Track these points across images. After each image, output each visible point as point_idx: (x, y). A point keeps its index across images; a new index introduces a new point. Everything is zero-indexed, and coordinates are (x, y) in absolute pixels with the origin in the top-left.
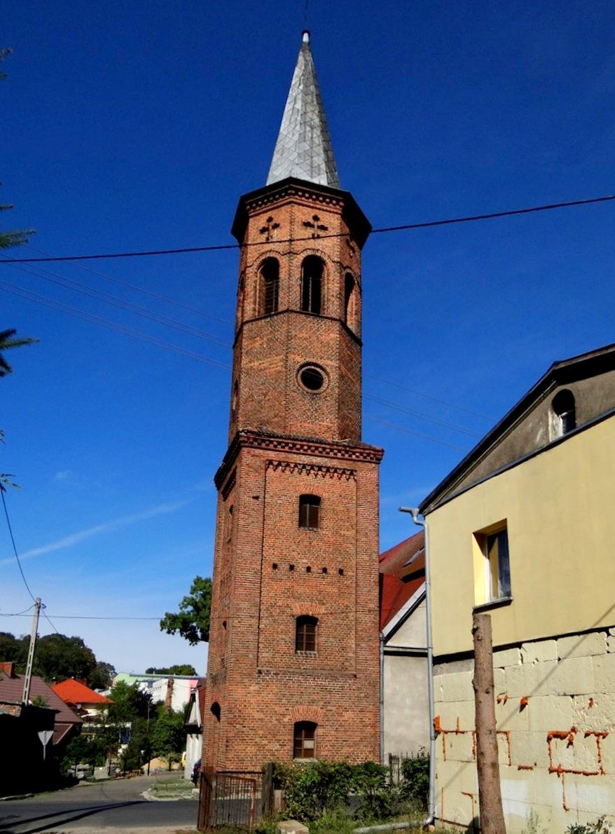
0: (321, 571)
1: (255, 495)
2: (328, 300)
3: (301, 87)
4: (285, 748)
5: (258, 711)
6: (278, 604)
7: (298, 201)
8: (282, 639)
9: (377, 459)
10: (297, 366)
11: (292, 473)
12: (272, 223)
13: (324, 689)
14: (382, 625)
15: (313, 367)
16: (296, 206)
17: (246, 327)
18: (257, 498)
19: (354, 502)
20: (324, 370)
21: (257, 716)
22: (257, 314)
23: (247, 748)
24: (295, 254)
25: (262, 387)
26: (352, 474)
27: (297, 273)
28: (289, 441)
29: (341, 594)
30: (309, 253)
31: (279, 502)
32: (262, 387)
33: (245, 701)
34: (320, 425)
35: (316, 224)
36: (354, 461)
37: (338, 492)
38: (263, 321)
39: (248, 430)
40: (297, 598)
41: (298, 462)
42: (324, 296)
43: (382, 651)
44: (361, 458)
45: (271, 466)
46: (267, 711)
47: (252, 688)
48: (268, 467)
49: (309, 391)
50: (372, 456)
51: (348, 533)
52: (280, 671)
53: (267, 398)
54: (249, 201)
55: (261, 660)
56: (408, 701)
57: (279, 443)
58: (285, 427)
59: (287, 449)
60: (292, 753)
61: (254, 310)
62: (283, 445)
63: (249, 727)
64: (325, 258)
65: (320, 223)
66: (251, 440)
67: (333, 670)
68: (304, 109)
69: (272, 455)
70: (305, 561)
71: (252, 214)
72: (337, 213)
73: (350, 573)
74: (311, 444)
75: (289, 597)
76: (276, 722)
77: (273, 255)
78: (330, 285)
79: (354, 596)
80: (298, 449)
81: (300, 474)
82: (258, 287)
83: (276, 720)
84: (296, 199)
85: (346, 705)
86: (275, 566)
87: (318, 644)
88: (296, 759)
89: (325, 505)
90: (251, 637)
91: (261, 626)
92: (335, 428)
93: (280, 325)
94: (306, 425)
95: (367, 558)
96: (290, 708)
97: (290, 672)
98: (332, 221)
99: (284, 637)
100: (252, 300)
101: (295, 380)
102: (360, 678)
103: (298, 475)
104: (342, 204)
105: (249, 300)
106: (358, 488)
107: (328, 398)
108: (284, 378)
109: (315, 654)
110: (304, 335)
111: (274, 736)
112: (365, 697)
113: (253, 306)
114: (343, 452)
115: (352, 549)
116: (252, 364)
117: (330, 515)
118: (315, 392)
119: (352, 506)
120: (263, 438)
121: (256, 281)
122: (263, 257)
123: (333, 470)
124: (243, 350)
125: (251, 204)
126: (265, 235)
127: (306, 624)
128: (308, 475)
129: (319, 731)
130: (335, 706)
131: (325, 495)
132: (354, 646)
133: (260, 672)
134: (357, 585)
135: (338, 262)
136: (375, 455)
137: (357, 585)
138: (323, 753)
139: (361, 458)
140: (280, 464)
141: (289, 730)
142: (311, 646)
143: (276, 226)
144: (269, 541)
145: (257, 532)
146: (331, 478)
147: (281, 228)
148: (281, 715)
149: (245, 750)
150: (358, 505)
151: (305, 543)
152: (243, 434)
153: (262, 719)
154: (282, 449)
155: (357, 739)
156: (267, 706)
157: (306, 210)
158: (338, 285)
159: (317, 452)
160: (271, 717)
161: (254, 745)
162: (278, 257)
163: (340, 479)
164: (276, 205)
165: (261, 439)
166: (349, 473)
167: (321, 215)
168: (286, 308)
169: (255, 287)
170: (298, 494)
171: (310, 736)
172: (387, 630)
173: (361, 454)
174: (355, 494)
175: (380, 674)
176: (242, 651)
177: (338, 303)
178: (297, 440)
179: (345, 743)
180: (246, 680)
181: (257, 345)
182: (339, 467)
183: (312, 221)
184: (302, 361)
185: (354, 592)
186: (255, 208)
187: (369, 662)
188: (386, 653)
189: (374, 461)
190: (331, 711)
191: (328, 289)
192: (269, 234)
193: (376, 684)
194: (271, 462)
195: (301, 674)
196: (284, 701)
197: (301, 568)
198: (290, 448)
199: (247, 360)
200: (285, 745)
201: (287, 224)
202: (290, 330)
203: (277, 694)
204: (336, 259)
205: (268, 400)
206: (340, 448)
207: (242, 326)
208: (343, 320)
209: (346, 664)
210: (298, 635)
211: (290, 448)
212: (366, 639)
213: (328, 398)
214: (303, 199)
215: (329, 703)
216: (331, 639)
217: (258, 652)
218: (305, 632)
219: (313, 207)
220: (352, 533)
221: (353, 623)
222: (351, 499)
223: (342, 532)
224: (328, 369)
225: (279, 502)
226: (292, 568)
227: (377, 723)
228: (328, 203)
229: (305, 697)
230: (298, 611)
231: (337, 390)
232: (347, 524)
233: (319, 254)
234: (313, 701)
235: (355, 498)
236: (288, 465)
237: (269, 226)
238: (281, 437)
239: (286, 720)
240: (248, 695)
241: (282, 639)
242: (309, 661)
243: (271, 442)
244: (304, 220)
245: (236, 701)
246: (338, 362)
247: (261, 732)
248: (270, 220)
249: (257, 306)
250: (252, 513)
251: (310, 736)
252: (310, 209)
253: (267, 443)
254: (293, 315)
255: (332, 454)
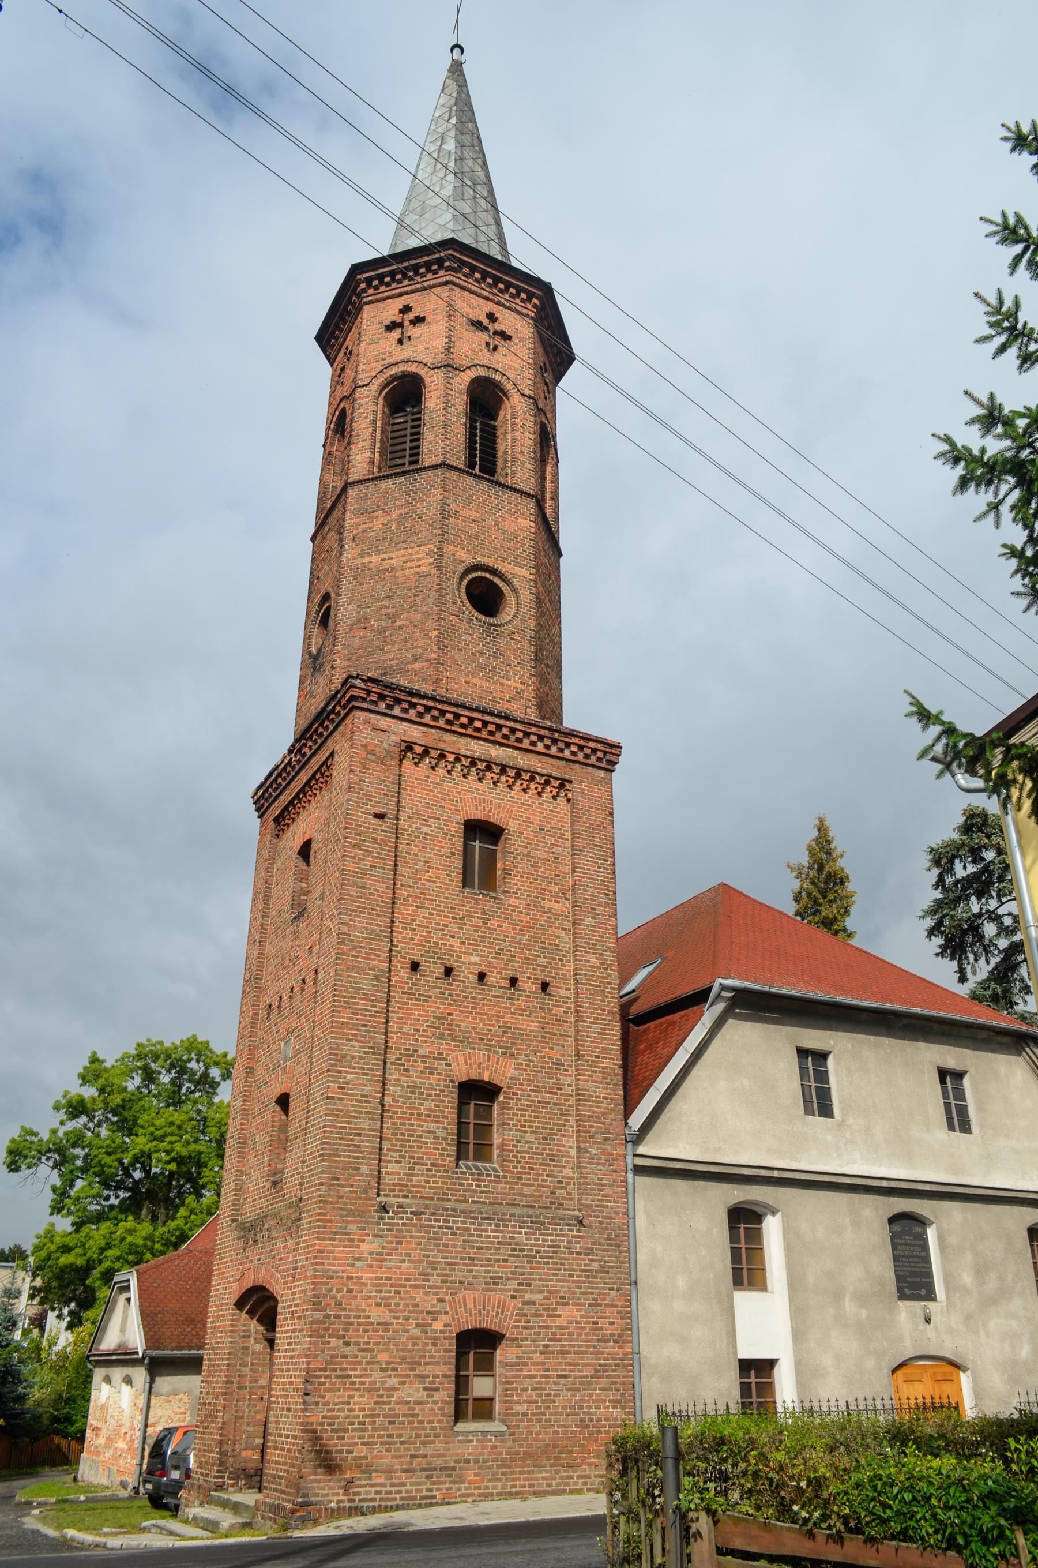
0: (506, 983)
1: (378, 810)
2: (514, 459)
3: (453, 121)
4: (437, 1396)
5: (378, 1305)
6: (421, 1051)
7: (462, 283)
8: (429, 1132)
9: (610, 762)
10: (461, 569)
11: (449, 772)
12: (411, 316)
13: (518, 1251)
14: (629, 1106)
15: (488, 575)
16: (458, 290)
17: (352, 493)
18: (380, 816)
19: (568, 844)
20: (507, 581)
21: (377, 1314)
22: (376, 470)
23: (351, 1397)
24: (456, 369)
25: (386, 602)
26: (562, 786)
27: (460, 403)
28: (448, 708)
29: (545, 1035)
30: (482, 372)
31: (425, 829)
32: (386, 602)
33: (350, 1278)
34: (502, 684)
35: (490, 327)
36: (567, 760)
37: (536, 819)
38: (390, 482)
39: (369, 678)
40: (463, 1040)
41: (463, 752)
42: (506, 452)
43: (630, 1166)
44: (580, 756)
45: (410, 755)
46: (397, 1305)
47: (365, 1247)
48: (404, 757)
49: (482, 617)
50: (600, 754)
51: (556, 906)
52: (427, 1206)
53: (398, 623)
54: (365, 275)
55: (386, 1180)
56: (681, 1282)
57: (428, 709)
58: (438, 681)
59: (442, 723)
60: (450, 1409)
61: (372, 462)
62: (436, 713)
63: (357, 1344)
64: (509, 386)
65: (498, 327)
66: (374, 697)
67: (533, 1207)
68: (459, 153)
69: (414, 733)
70: (474, 959)
71: (370, 298)
72: (527, 316)
73: (563, 992)
74: (488, 718)
75: (442, 1037)
76: (415, 1332)
77: (412, 368)
78: (517, 434)
79: (571, 1041)
80: (463, 726)
81: (465, 776)
82: (379, 424)
83: (418, 1325)
84: (459, 279)
85: (563, 1288)
86: (415, 966)
87: (502, 1147)
88: (458, 1425)
89: (513, 843)
90: (366, 1124)
91: (388, 1100)
92: (530, 693)
93: (429, 492)
94: (475, 681)
95: (594, 961)
96: (448, 1298)
97: (447, 1210)
98: (519, 326)
99: (433, 1126)
100: (368, 444)
101: (457, 593)
102: (590, 1227)
103: (462, 779)
104: (535, 301)
105: (361, 445)
106: (574, 817)
107: (515, 636)
108: (436, 587)
109: (495, 1170)
110: (473, 513)
111: (414, 1365)
112: (602, 1270)
113: (368, 454)
114: (548, 742)
115: (565, 941)
116: (366, 560)
117: (523, 866)
118: (492, 620)
119: (564, 850)
120: (399, 695)
121: (375, 413)
122: (392, 371)
123: (485, 764)
124: (346, 534)
125: (369, 281)
126: (396, 334)
127: (478, 1094)
128: (480, 780)
129: (503, 1355)
130: (542, 1292)
131: (512, 825)
132: (573, 1152)
133: (384, 1208)
134: (579, 1019)
135: (530, 397)
136: (605, 753)
137: (579, 1019)
138: (517, 1408)
139: (580, 756)
140: (426, 752)
141: (445, 1351)
142: (483, 1152)
143: (419, 320)
144: (404, 912)
145: (383, 889)
146: (524, 790)
147: (429, 323)
148: (428, 1313)
149: (349, 1403)
150: (575, 850)
151: (475, 922)
152: (358, 682)
153: (386, 1324)
154: (432, 723)
155: (588, 1372)
156: (396, 1292)
157: (475, 300)
158: (531, 436)
159: (498, 737)
160: (407, 1319)
161: (369, 1390)
162: (422, 372)
163: (539, 794)
164: (418, 286)
165: (389, 695)
166: (557, 783)
167: (500, 312)
168: (439, 460)
169: (375, 421)
170: (461, 818)
171: (486, 1366)
172: (637, 1119)
173: (581, 748)
174: (568, 827)
175: (629, 1215)
176: (347, 1157)
177: (531, 467)
178: (463, 706)
179: (563, 1381)
180: (352, 1228)
181: (377, 524)
182: (539, 770)
183: (485, 322)
184: (469, 560)
185: (572, 1032)
186: (376, 288)
187: (608, 1190)
188: (639, 1170)
189: (603, 765)
190: (534, 1303)
191: (514, 440)
192: (402, 333)
193: (620, 1241)
194: (409, 747)
195: (468, 1214)
196: (435, 1279)
197: (467, 975)
198: (449, 722)
199: (356, 551)
200: (437, 1390)
201: (442, 317)
202: (448, 502)
203: (420, 1261)
204: (527, 392)
205: (400, 628)
206: (542, 732)
207: (344, 489)
208: (539, 497)
209: (559, 1192)
210: (461, 1126)
211: (449, 722)
212: (599, 1137)
213: (515, 636)
214: (471, 281)
215: (529, 1285)
216: (529, 1136)
217: (380, 1160)
218: (472, 1120)
219: (487, 298)
220: (564, 907)
221: (572, 1101)
222: (562, 837)
223: (547, 904)
224: (516, 583)
225: (425, 829)
226: (448, 971)
227: (626, 1332)
228: (512, 296)
229: (479, 1270)
230: (462, 1071)
231: (532, 623)
232: (555, 888)
233: (497, 377)
234: (495, 1281)
235: (568, 835)
236: (442, 756)
237: (403, 319)
238: (433, 699)
239: (438, 1325)
240: (358, 1264)
241: (429, 1132)
242: (478, 1183)
243: (413, 705)
244: (470, 316)
245: (332, 1277)
246: (533, 571)
247: (383, 1357)
248: (406, 309)
249: (377, 455)
250: (372, 847)
251: (486, 1366)
252: (481, 300)
253: (405, 705)
254: (452, 475)
255: (526, 743)
